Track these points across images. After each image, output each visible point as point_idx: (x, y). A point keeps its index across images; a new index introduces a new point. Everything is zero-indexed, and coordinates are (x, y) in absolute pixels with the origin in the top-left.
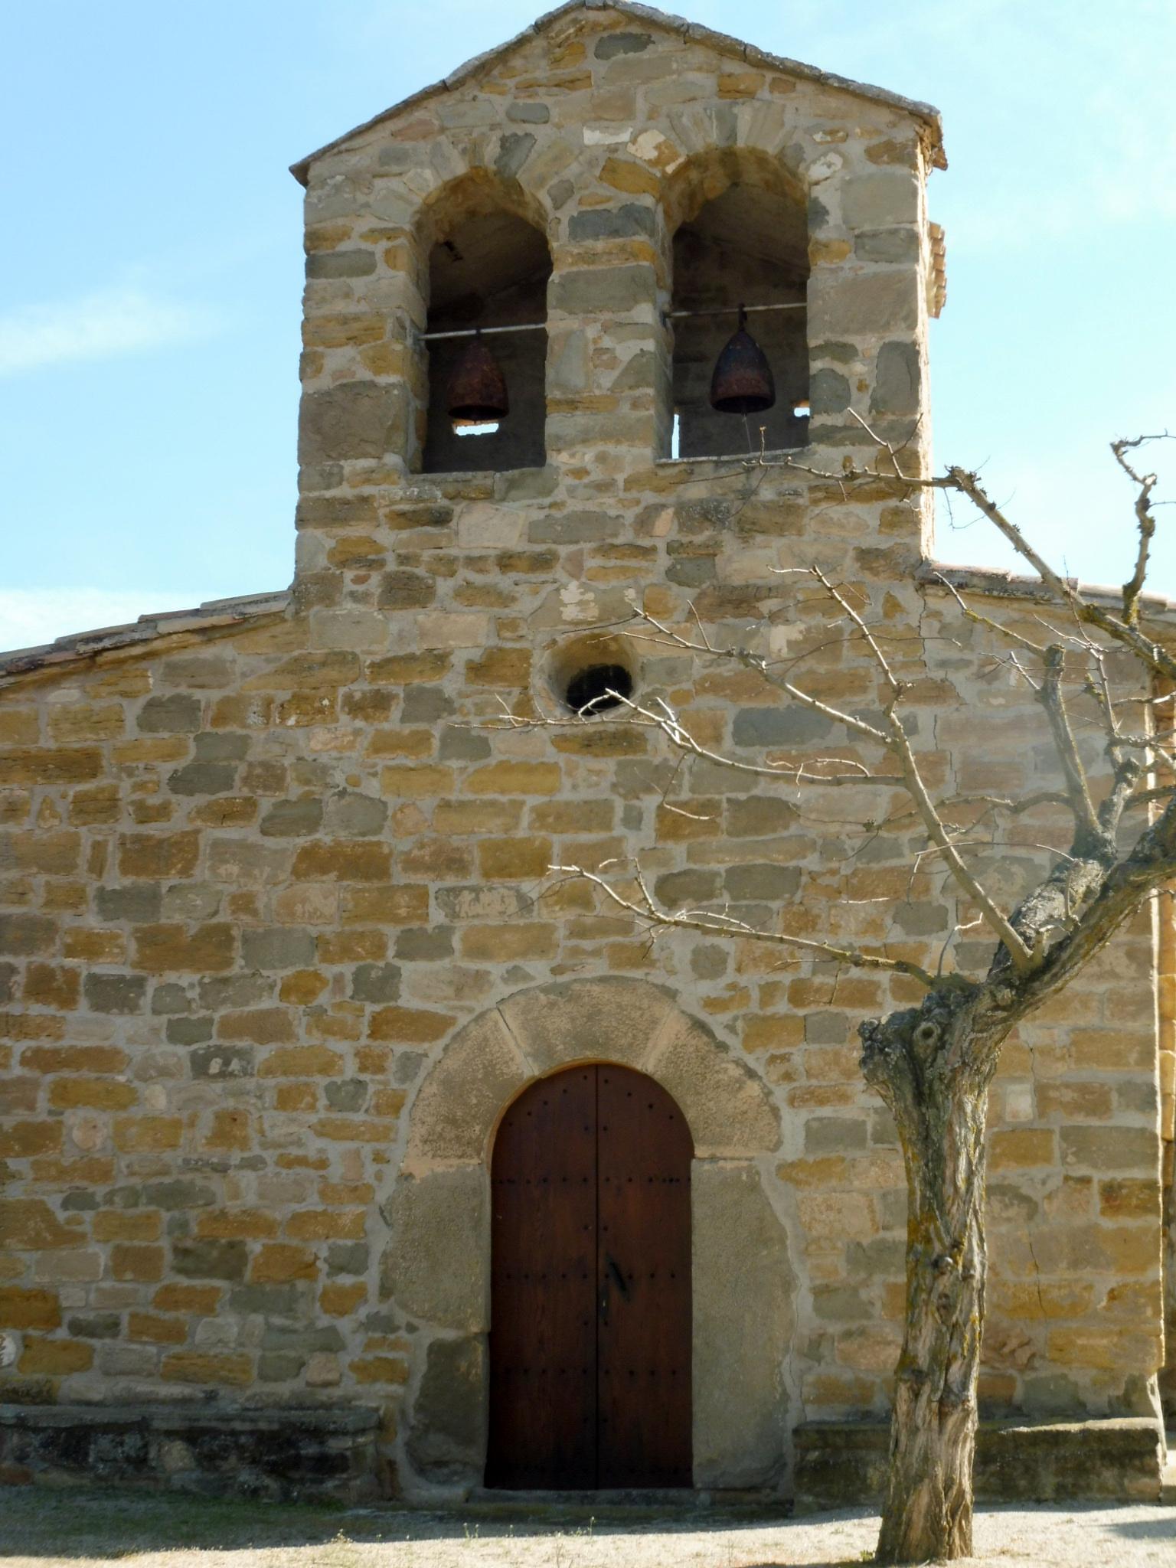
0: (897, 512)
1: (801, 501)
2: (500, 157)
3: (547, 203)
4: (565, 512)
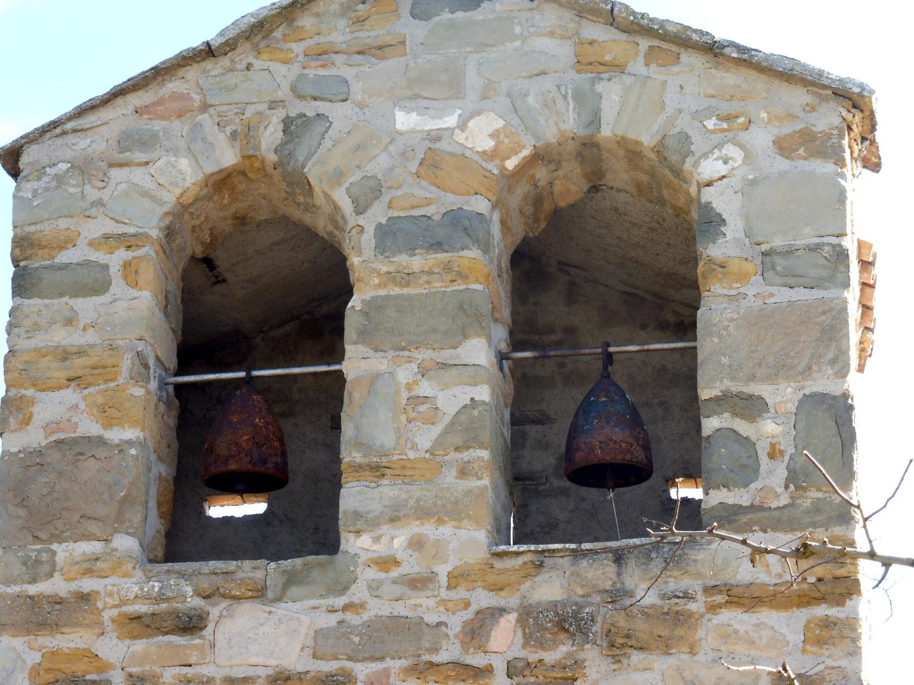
0: (827, 624)
1: (693, 606)
2: (284, 144)
3: (347, 206)
4: (366, 616)
